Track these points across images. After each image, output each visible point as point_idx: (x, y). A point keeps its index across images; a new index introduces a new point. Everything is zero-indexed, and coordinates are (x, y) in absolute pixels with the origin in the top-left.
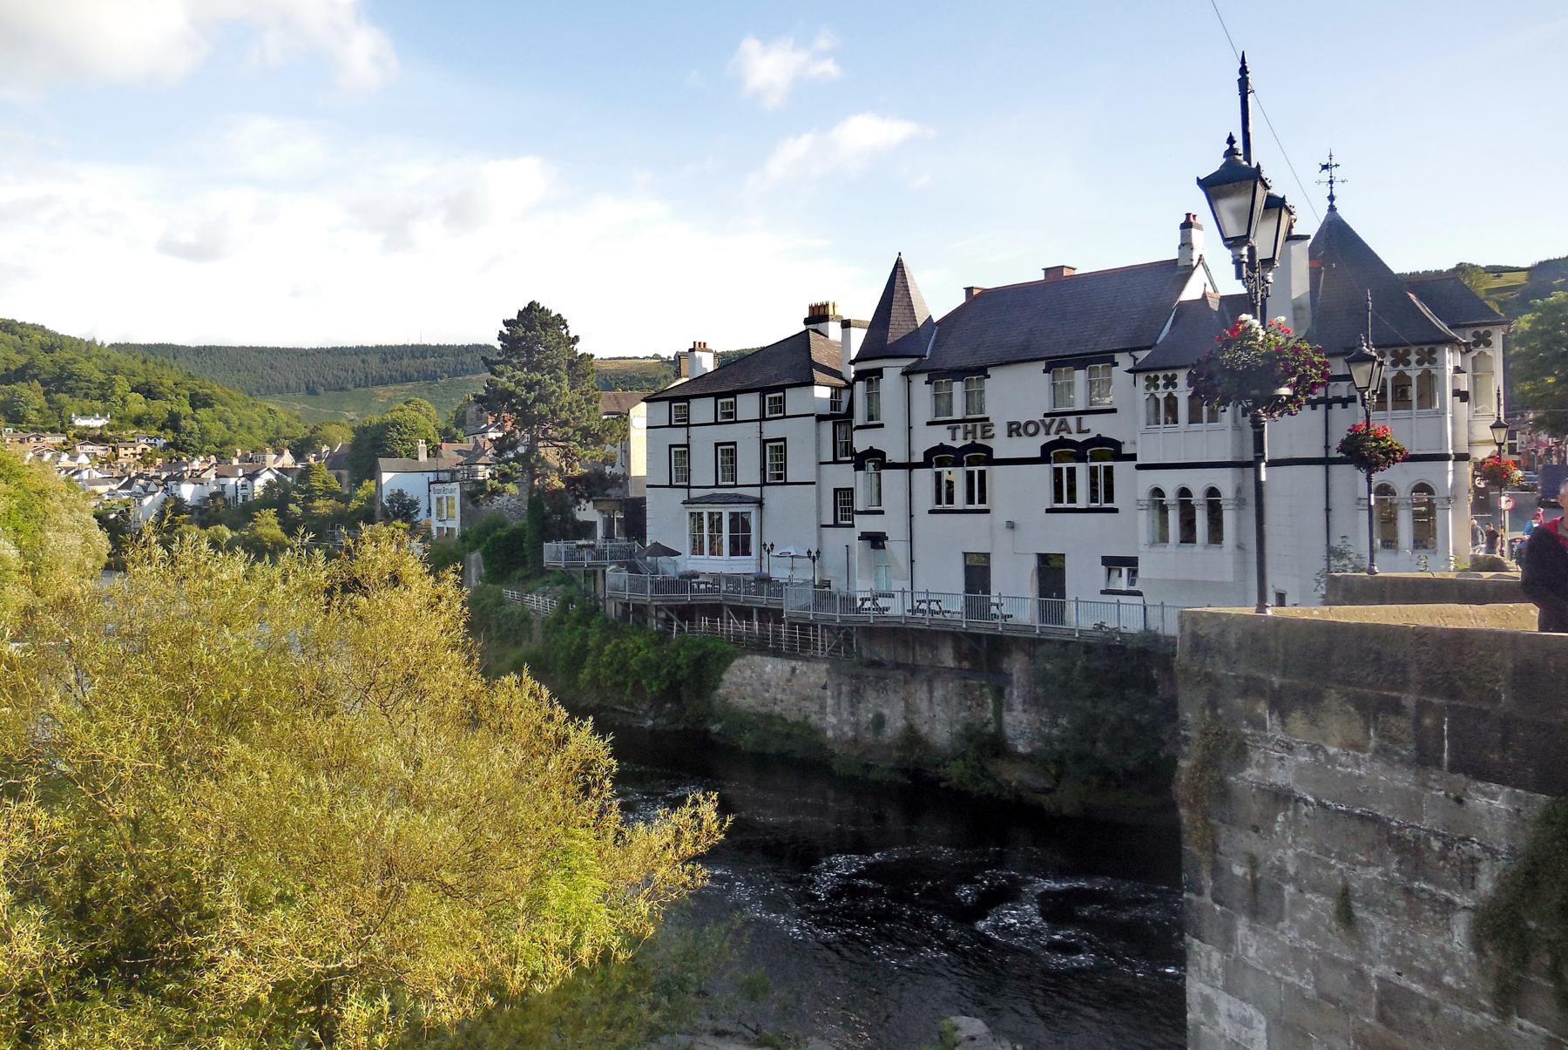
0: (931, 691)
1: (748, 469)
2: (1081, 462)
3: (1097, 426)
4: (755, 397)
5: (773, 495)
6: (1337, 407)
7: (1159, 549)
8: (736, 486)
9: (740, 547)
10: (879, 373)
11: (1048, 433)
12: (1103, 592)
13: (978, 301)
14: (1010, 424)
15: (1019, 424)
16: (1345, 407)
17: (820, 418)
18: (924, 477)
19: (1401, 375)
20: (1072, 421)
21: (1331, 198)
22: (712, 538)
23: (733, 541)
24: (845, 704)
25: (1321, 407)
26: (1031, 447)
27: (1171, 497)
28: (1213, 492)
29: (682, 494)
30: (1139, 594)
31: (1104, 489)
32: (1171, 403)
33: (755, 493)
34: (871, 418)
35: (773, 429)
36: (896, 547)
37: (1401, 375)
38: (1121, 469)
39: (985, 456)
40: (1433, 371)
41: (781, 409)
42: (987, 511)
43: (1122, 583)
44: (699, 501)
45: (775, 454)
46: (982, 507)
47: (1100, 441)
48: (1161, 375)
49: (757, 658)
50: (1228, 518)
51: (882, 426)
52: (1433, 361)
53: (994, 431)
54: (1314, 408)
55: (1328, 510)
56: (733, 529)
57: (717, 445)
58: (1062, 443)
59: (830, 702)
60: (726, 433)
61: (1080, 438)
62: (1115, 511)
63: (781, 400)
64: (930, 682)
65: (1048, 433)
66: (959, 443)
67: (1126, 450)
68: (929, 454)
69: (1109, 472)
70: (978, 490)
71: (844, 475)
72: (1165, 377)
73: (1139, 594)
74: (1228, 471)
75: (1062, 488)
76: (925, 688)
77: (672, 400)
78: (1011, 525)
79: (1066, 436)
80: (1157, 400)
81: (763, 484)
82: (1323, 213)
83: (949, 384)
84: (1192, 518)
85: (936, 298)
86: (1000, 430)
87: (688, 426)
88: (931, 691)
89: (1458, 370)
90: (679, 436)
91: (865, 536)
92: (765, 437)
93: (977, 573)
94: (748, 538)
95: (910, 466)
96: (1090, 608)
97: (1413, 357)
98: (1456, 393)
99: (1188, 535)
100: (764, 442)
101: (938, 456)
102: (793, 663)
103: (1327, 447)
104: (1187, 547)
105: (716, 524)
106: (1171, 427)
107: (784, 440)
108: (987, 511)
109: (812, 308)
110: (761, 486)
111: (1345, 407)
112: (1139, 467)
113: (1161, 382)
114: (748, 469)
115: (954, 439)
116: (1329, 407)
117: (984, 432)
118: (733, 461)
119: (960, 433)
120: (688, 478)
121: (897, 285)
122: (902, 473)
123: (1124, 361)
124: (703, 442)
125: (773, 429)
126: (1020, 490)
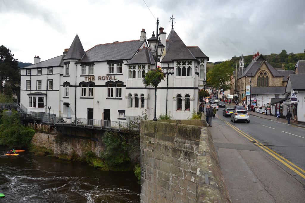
1: (44, 87)
2: (114, 86)
3: (119, 78)
5: (50, 93)
6: (170, 75)
8: (41, 91)
9: (41, 105)
10: (69, 63)
11: (107, 79)
12: (118, 119)
14: (99, 77)
16: (172, 75)
18: (79, 89)
19: (184, 67)
20: (113, 77)
21: (173, 26)
22: (34, 103)
23: (39, 104)
24: (58, 145)
26: (103, 83)
27: (133, 96)
28: (187, 96)
29: (29, 92)
31: (119, 93)
32: (134, 72)
33: (45, 92)
34: (67, 74)
35: (50, 77)
36: (72, 106)
37: (184, 67)
40: (191, 67)
41: (52, 72)
42: (93, 98)
43: (122, 117)
44: (33, 94)
45: (50, 82)
46: (92, 97)
47: (119, 81)
48: (142, 65)
49: (40, 134)
50: (146, 101)
51: (69, 76)
52: (191, 64)
53: (95, 78)
55: (167, 100)
56: (39, 100)
57: (37, 80)
58: (110, 82)
60: (39, 78)
61: (114, 81)
65: (107, 79)
66: (87, 81)
67: (124, 84)
68: (80, 83)
70: (91, 92)
72: (143, 66)
74: (193, 90)
75: (110, 93)
78: (98, 102)
79: (111, 80)
80: (131, 72)
81: (47, 90)
83: (86, 66)
87: (31, 75)
90: (28, 78)
92: (48, 79)
93: (90, 112)
94: (36, 103)
95: (76, 86)
99: (137, 106)
101: (83, 84)
102: (48, 135)
103: (167, 85)
104: (136, 108)
105: (35, 100)
108: (93, 98)
109: (65, 50)
110: (47, 91)
111: (172, 75)
112: (126, 88)
113: (132, 67)
114: (44, 87)
115: (86, 80)
116: (168, 75)
117: (93, 79)
119: (87, 79)
120: (30, 89)
121: (77, 42)
122: (169, 86)
123: (125, 62)
124: (34, 79)
125: (50, 77)
126: (101, 93)
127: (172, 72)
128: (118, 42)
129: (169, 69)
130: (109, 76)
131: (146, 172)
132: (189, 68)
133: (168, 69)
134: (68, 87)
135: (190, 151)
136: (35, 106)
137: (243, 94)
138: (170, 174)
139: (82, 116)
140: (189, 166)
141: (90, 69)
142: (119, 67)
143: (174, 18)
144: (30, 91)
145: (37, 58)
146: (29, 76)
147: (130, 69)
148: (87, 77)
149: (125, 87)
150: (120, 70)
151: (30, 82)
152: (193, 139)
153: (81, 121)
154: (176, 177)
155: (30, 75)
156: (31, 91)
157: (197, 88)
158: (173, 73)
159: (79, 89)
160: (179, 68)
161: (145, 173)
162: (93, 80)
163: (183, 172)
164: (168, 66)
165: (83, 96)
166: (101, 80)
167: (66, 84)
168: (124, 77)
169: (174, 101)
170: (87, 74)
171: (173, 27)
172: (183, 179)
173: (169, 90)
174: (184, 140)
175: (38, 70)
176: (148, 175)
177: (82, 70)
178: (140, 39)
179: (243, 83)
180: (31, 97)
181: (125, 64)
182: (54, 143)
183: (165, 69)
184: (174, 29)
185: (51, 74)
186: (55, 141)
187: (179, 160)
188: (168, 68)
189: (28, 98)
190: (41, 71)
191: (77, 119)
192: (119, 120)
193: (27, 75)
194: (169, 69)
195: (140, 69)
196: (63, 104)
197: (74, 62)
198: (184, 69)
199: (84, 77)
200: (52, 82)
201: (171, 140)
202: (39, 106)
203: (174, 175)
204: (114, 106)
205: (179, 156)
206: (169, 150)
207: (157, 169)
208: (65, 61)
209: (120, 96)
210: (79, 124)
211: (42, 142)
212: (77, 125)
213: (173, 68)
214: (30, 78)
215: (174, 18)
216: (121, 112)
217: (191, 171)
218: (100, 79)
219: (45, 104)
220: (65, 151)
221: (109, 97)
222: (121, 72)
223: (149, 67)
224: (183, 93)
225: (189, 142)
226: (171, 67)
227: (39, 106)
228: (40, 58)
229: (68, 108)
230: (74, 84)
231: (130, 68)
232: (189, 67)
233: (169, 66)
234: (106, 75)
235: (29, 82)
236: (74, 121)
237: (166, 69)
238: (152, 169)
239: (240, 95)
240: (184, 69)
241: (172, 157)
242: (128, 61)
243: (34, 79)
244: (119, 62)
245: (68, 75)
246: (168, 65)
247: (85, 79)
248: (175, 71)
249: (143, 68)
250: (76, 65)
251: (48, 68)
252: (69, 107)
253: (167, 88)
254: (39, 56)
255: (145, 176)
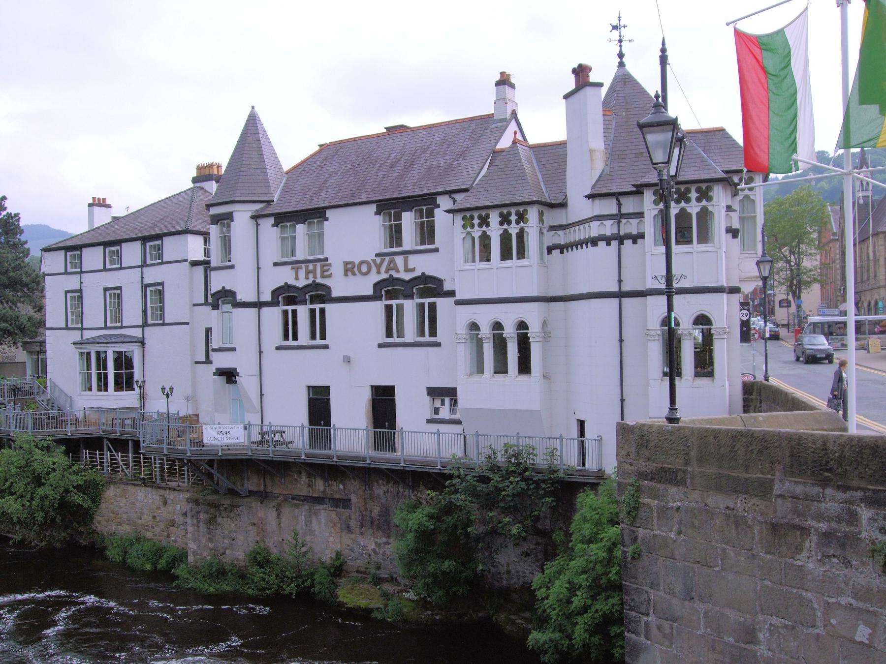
0: (279, 516)
1: (132, 312)
2: (409, 294)
3: (422, 265)
4: (137, 245)
5: (153, 335)
6: (628, 243)
7: (476, 379)
8: (122, 327)
9: (125, 382)
10: (229, 217)
11: (379, 272)
13: (330, 153)
14: (346, 264)
15: (353, 263)
16: (635, 242)
17: (194, 264)
18: (273, 316)
20: (399, 260)
21: (621, 56)
23: (117, 377)
24: (203, 527)
25: (614, 243)
27: (486, 331)
29: (76, 336)
30: (458, 422)
31: (429, 323)
32: (485, 240)
33: (137, 333)
35: (152, 275)
36: (247, 379)
38: (443, 304)
39: (320, 294)
40: (710, 209)
41: (160, 256)
45: (155, 293)
46: (323, 342)
48: (476, 215)
52: (709, 199)
54: (608, 244)
56: (118, 364)
57: (106, 290)
58: (392, 281)
59: (190, 529)
61: (407, 277)
62: (438, 344)
63: (160, 248)
64: (278, 508)
65: (379, 272)
66: (302, 283)
67: (447, 287)
68: (276, 293)
69: (433, 307)
70: (318, 327)
71: (210, 317)
72: (480, 217)
73: (458, 422)
76: (275, 514)
77: (67, 249)
78: (347, 360)
79: (395, 275)
80: (473, 239)
81: (145, 325)
82: (613, 69)
84: (514, 351)
85: (291, 147)
86: (337, 269)
87: (81, 272)
88: (279, 516)
89: (729, 208)
90: (72, 283)
91: (220, 372)
92: (145, 282)
93: (319, 405)
95: (259, 305)
96: (420, 437)
97: (693, 195)
98: (729, 230)
99: (501, 369)
100: (145, 287)
101: (287, 295)
103: (620, 281)
104: (500, 378)
105: (102, 362)
106: (486, 265)
107: (162, 284)
109: (199, 168)
110: (143, 326)
111: (635, 242)
112: (458, 303)
114: (132, 312)
115: (297, 278)
116: (621, 243)
117: (323, 271)
118: (120, 304)
119: (302, 273)
121: (252, 135)
122: (253, 311)
123: (445, 203)
124: (94, 288)
125: (152, 275)
126: (355, 325)
127: (635, 232)
128: (402, 127)
129: (624, 221)
130: (387, 259)
131: (648, 615)
132: (705, 216)
133: (619, 222)
134: (227, 307)
135: (844, 528)
136: (103, 386)
137: (876, 303)
138: (760, 617)
139: (290, 418)
140: (843, 586)
141: (310, 236)
142: (422, 224)
143: (625, 26)
144: (82, 329)
145: (99, 203)
146: (608, 240)
147: (505, 226)
148: (301, 268)
149: (452, 299)
150: (427, 233)
151: (81, 298)
152: (855, 483)
153: (287, 437)
154: (786, 626)
155: (78, 270)
156: (84, 331)
157: (735, 290)
158: (642, 236)
159: (273, 316)
160: (664, 215)
161: (646, 618)
162: (323, 277)
163: (816, 606)
164: (620, 210)
165: (422, 334)
166: (354, 274)
167: (223, 298)
168: (449, 256)
169: (650, 344)
170: (300, 256)
171: (624, 60)
172: (818, 634)
173: (625, 301)
174: (816, 490)
175: (148, 245)
176: (659, 628)
177: (280, 240)
178: (492, 112)
179: (876, 261)
180: (89, 354)
181: (449, 211)
182: (185, 524)
183: (608, 223)
184: (630, 67)
185: (158, 264)
186: (189, 515)
187: (799, 563)
188: (619, 217)
189: (78, 356)
190: (119, 253)
191: (274, 429)
192: (434, 427)
193: (66, 273)
194: (624, 221)
195: (469, 229)
196: (215, 374)
197: (250, 214)
198: (683, 216)
199: (289, 267)
200: (161, 293)
201: (763, 489)
202: (119, 386)
203: (776, 621)
204: (411, 374)
205: (799, 549)
206: (749, 527)
207: (701, 600)
208: (214, 211)
209: (433, 333)
210: (278, 448)
211: (140, 522)
212: (273, 451)
213: (640, 215)
214: (81, 283)
215: (625, 26)
216: (444, 394)
217: (853, 601)
218: (349, 273)
219: (137, 376)
220: (228, 552)
221: (313, 343)
222: (432, 240)
223: (541, 214)
224: (509, 316)
225: (840, 495)
226: (632, 211)
227: (119, 386)
228: (109, 206)
229: (231, 386)
230: (253, 298)
231: (468, 222)
232: (484, 233)
233: (624, 210)
234: (374, 258)
235: (77, 297)
236: (259, 438)
237: (611, 222)
238: (675, 601)
239: (865, 304)
240: (683, 216)
241: (767, 553)
242: (459, 197)
243: (94, 288)
244: (424, 203)
245: (229, 264)
246: (620, 204)
247: (293, 273)
248: (649, 226)
249: (480, 226)
250: (258, 225)
251: (145, 239)
252: (235, 382)
253: (620, 295)
254: (104, 200)
255: (647, 632)
